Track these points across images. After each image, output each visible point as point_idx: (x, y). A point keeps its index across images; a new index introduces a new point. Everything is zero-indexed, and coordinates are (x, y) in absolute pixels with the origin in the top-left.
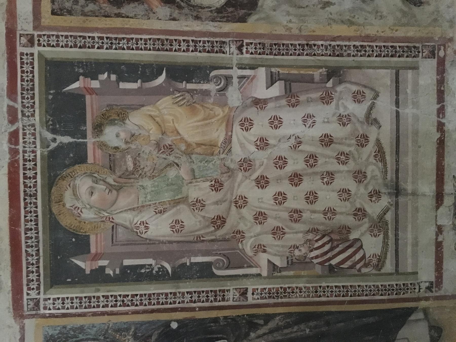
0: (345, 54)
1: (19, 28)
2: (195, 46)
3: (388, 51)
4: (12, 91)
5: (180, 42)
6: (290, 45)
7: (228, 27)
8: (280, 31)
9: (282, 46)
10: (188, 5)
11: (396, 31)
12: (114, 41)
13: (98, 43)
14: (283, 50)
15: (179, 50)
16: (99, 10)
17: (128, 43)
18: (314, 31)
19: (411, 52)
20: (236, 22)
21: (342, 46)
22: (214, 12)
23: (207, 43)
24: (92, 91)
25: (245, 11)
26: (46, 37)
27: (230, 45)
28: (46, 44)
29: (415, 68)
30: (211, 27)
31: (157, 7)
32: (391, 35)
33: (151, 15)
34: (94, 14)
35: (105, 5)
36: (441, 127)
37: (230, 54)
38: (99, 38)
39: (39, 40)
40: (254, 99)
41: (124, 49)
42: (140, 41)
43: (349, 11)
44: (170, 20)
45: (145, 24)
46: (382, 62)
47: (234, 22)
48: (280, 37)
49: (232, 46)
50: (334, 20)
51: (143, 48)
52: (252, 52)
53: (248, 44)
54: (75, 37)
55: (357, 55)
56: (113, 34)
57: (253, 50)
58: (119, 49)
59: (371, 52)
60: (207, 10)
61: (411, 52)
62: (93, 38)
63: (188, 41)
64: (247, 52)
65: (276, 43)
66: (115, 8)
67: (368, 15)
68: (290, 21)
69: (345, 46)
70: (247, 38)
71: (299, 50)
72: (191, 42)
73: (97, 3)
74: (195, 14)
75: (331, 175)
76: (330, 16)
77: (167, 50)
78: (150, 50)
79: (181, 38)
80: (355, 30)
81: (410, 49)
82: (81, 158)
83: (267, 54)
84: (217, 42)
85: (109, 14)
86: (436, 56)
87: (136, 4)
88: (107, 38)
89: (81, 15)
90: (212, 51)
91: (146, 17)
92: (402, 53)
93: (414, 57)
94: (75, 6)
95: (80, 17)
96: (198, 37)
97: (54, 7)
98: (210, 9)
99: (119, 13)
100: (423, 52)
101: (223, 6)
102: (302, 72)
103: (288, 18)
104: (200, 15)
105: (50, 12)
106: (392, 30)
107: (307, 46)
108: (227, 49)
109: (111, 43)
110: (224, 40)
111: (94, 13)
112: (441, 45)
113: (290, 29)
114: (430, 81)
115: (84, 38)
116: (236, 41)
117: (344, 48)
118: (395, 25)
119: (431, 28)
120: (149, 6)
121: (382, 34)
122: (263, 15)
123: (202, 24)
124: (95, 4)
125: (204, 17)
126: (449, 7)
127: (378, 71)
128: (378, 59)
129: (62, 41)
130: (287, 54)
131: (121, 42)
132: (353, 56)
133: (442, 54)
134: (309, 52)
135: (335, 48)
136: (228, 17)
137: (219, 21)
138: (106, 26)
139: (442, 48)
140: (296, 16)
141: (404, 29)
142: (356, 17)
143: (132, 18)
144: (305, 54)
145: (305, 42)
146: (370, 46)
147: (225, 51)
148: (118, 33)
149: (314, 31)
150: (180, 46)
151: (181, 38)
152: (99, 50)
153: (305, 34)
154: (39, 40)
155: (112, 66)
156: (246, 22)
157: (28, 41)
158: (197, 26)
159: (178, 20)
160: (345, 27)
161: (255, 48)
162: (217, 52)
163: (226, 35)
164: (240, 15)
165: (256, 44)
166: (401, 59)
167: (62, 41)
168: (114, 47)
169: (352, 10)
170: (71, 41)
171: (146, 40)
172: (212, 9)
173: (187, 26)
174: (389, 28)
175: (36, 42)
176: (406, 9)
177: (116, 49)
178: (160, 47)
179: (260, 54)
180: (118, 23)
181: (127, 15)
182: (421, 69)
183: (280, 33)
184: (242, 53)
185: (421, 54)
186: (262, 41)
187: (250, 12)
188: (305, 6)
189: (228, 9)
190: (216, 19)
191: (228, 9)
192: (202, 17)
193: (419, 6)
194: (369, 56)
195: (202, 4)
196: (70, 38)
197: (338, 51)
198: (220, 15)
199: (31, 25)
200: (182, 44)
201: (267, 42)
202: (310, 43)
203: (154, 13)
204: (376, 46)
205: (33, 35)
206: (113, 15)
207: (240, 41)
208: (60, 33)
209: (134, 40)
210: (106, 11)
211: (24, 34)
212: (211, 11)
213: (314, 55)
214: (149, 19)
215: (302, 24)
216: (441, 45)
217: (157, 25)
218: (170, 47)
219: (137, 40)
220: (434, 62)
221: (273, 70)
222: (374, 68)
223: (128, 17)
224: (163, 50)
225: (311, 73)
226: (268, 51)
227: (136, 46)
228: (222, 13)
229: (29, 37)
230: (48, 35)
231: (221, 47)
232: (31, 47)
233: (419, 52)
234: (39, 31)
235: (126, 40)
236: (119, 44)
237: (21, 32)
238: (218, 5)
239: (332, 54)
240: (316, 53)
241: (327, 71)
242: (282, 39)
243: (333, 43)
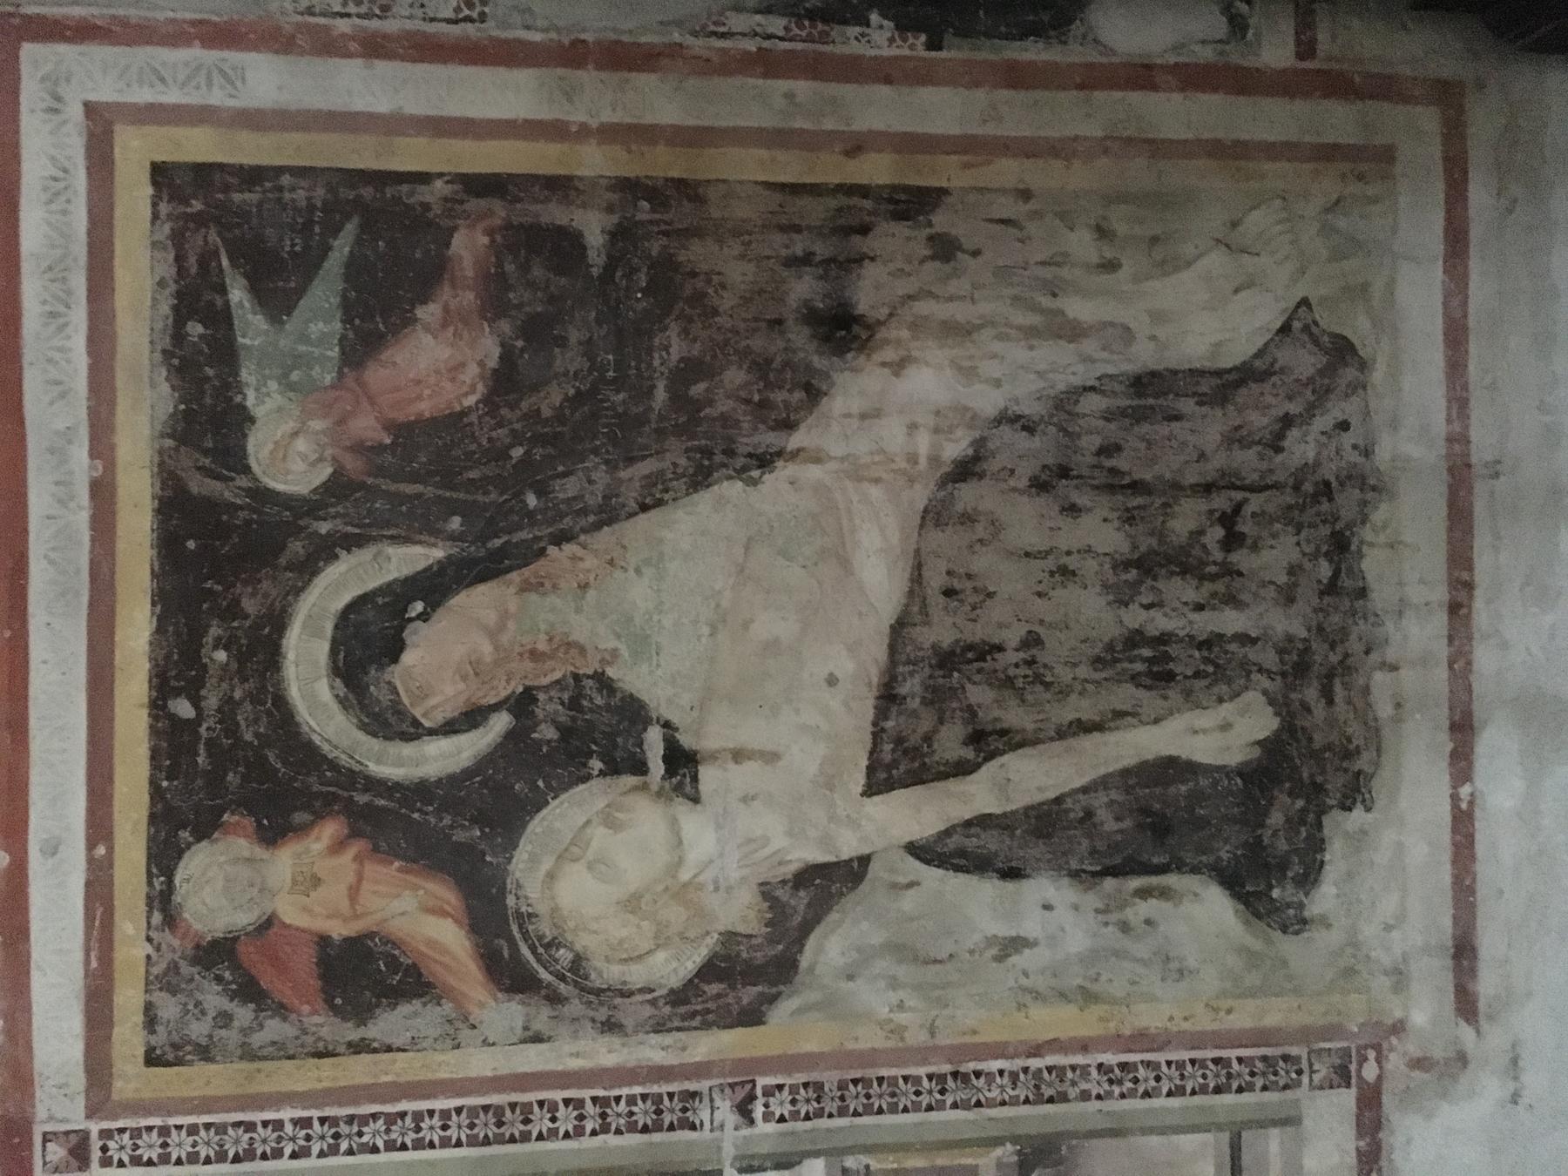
0: (1073, 1093)
1: (41, 1112)
2: (603, 1116)
3: (1204, 1076)
5: (553, 1107)
6: (901, 1081)
7: (706, 1045)
8: (870, 1039)
9: (875, 1084)
10: (582, 990)
11: (1229, 1011)
12: (344, 1129)
13: (293, 1139)
14: (880, 1096)
15: (553, 1133)
16: (297, 1038)
17: (388, 1131)
18: (975, 1032)
19: (1276, 1074)
20: (731, 1026)
21: (1064, 1068)
22: (661, 1002)
23: (640, 1102)
25: (760, 988)
26: (127, 1136)
27: (712, 1100)
28: (126, 1159)
29: (1289, 1121)
30: (654, 1051)
31: (482, 1005)
32: (1215, 1026)
33: (465, 1034)
34: (281, 1051)
35: (317, 1019)
36: (1458, 440)
37: (712, 1130)
38: (297, 1122)
39: (104, 1149)
41: (375, 1150)
42: (427, 1119)
43: (1081, 961)
44: (524, 1041)
46: (1185, 1109)
47: (725, 1027)
48: (871, 1057)
49: (718, 1103)
50: (1037, 996)
51: (437, 1142)
52: (782, 1116)
53: (768, 1092)
54: (221, 1129)
55: (1109, 1094)
56: (340, 1105)
57: (786, 1110)
58: (361, 1152)
59: (1153, 1083)
60: (639, 998)
61: (1276, 1074)
62: (278, 1125)
63: (580, 1104)
64: (767, 1117)
65: (858, 1076)
66: (350, 1025)
67: (1140, 970)
68: (901, 1006)
69: (1073, 1068)
70: (764, 1074)
71: (930, 1092)
72: (589, 1103)
73: (293, 1016)
74: (602, 1014)
76: (1024, 981)
77: (512, 1140)
78: (459, 1144)
79: (558, 1095)
80: (1101, 1019)
81: (1273, 1065)
83: (830, 1116)
84: (671, 1095)
85: (330, 1048)
86: (1353, 1081)
87: (417, 1004)
88: (322, 1120)
89: (241, 1058)
90: (658, 1127)
91: (449, 1041)
92: (1248, 1078)
93: (1286, 1087)
94: (223, 1032)
95: (236, 1066)
96: (612, 1087)
97: (153, 1043)
98: (649, 997)
99: (363, 1039)
100: (1312, 1072)
101: (691, 981)
102: (940, 1162)
103: (894, 997)
104: (620, 1016)
105: (141, 1060)
106: (1216, 1010)
107: (957, 1080)
108: (705, 1115)
109: (336, 1136)
110: (692, 1086)
111: (279, 1050)
112: (1366, 1047)
113: (898, 1031)
114: (1336, 1159)
115: (250, 1127)
116: (732, 1086)
117: (1070, 1075)
118: (1224, 994)
119: (1336, 998)
120: (459, 1005)
121: (1186, 1026)
122: (813, 996)
123: (623, 1045)
124: (285, 1019)
125: (629, 1023)
126: (1388, 928)
127: (1175, 1138)
128: (1175, 1102)
129: (179, 1145)
130: (893, 1109)
131: (365, 1129)
132: (1099, 1097)
133: (1370, 1072)
134: (961, 1096)
135: (1041, 1078)
136: (708, 1011)
137: (679, 1029)
138: (319, 1086)
139: (1371, 1054)
140: (918, 987)
141: (1251, 1004)
142: (1104, 978)
143: (404, 1050)
144: (949, 1103)
145: (946, 1068)
146: (1147, 1064)
147: (698, 1123)
148: (355, 1102)
149: (975, 1032)
150: (553, 1119)
151: (558, 1095)
152: (296, 1164)
153: (948, 1042)
154: (104, 1149)
156: (764, 1023)
157: (71, 1152)
158: (607, 1053)
159: (549, 1039)
160: (1071, 1010)
161: (794, 1102)
162: (671, 1128)
163: (700, 1070)
164: (745, 1001)
165: (794, 1089)
166: (1246, 1097)
167: (181, 1145)
168: (344, 1146)
169: (1091, 958)
170: (208, 1144)
171: (446, 1115)
172: (656, 994)
173: (577, 1055)
174: (1207, 1005)
175: (96, 1154)
176: (1256, 945)
177: (350, 1152)
178: (492, 1131)
179: (807, 1118)
180: (359, 1070)
181: (388, 1041)
182: (1307, 1122)
183: (869, 1045)
184: (752, 1122)
185: (1305, 1079)
186: (814, 1076)
187: (774, 990)
188: (944, 955)
189: (706, 988)
190: (669, 1025)
191: (706, 988)
192: (625, 1022)
193: (1297, 933)
194: (1147, 1094)
195: (625, 983)
196: (203, 1133)
197: (1050, 1085)
198: (682, 1010)
199: (81, 1102)
200: (562, 1112)
201: (830, 1078)
202: (962, 1069)
203: (474, 1027)
204: (1169, 1063)
205: (84, 1136)
206: (342, 1049)
207: (743, 1083)
208: (172, 1121)
209: (408, 1120)
210: (320, 1039)
211: (55, 1134)
212: (653, 1002)
213: (979, 1104)
214: (458, 1047)
215: (934, 1013)
216: (1366, 1047)
217: (480, 1063)
218: (522, 1127)
219: (418, 1117)
220: (1347, 1098)
221: (850, 1162)
222: (1163, 1131)
223: (389, 1049)
224: (500, 1140)
225: (970, 1161)
226: (832, 1107)
227: (415, 1136)
228: (686, 1002)
229: (74, 1139)
230: (132, 1130)
231: (685, 1110)
232: (80, 1169)
233: (1299, 1072)
234: (106, 1118)
235: (381, 1122)
236: (360, 1134)
237: (49, 1128)
238: (675, 982)
239: (1031, 1097)
240: (983, 1100)
241: (1019, 1153)
242: (873, 1065)
243: (1035, 1063)
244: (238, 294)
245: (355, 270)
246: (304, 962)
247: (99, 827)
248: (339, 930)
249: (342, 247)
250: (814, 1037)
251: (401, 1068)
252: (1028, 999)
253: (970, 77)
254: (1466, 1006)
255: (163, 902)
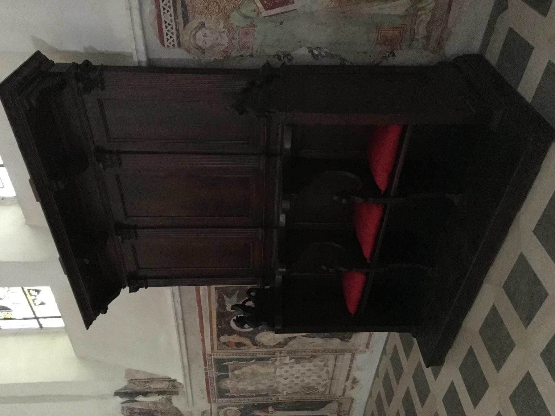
4: (205, 364)
7: (276, 349)
24: (230, 364)
30: (271, 350)
40: (241, 84)
45: (248, 350)
75: (310, 376)
82: (227, 376)
155: (236, 359)
158: (266, 350)
217: (251, 350)
244: (225, 297)
245: (238, 294)
246: (234, 344)
247: (212, 335)
248: (237, 342)
249: (237, 292)
250: (289, 349)
251: (245, 351)
252: (172, 389)
253: (299, 357)
254: (367, 347)
255: (218, 339)
